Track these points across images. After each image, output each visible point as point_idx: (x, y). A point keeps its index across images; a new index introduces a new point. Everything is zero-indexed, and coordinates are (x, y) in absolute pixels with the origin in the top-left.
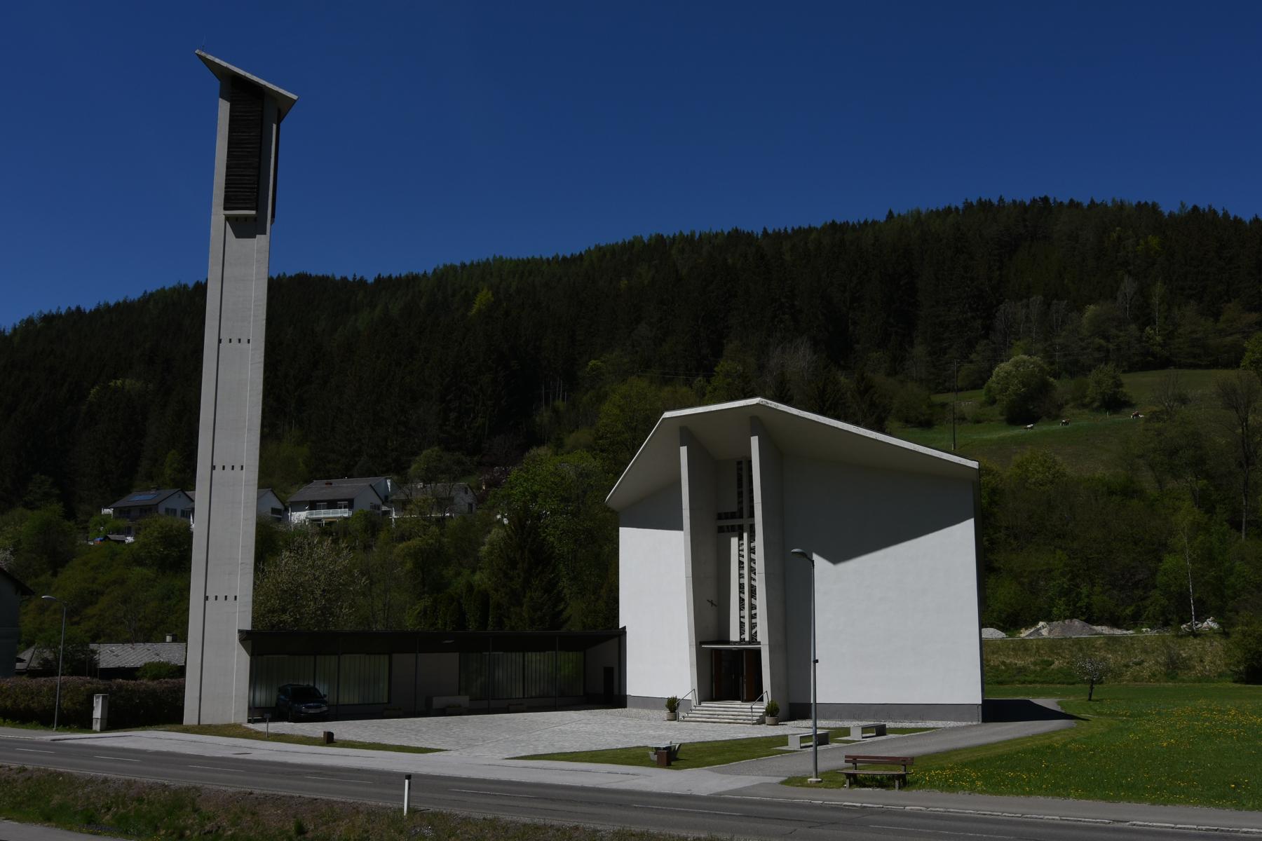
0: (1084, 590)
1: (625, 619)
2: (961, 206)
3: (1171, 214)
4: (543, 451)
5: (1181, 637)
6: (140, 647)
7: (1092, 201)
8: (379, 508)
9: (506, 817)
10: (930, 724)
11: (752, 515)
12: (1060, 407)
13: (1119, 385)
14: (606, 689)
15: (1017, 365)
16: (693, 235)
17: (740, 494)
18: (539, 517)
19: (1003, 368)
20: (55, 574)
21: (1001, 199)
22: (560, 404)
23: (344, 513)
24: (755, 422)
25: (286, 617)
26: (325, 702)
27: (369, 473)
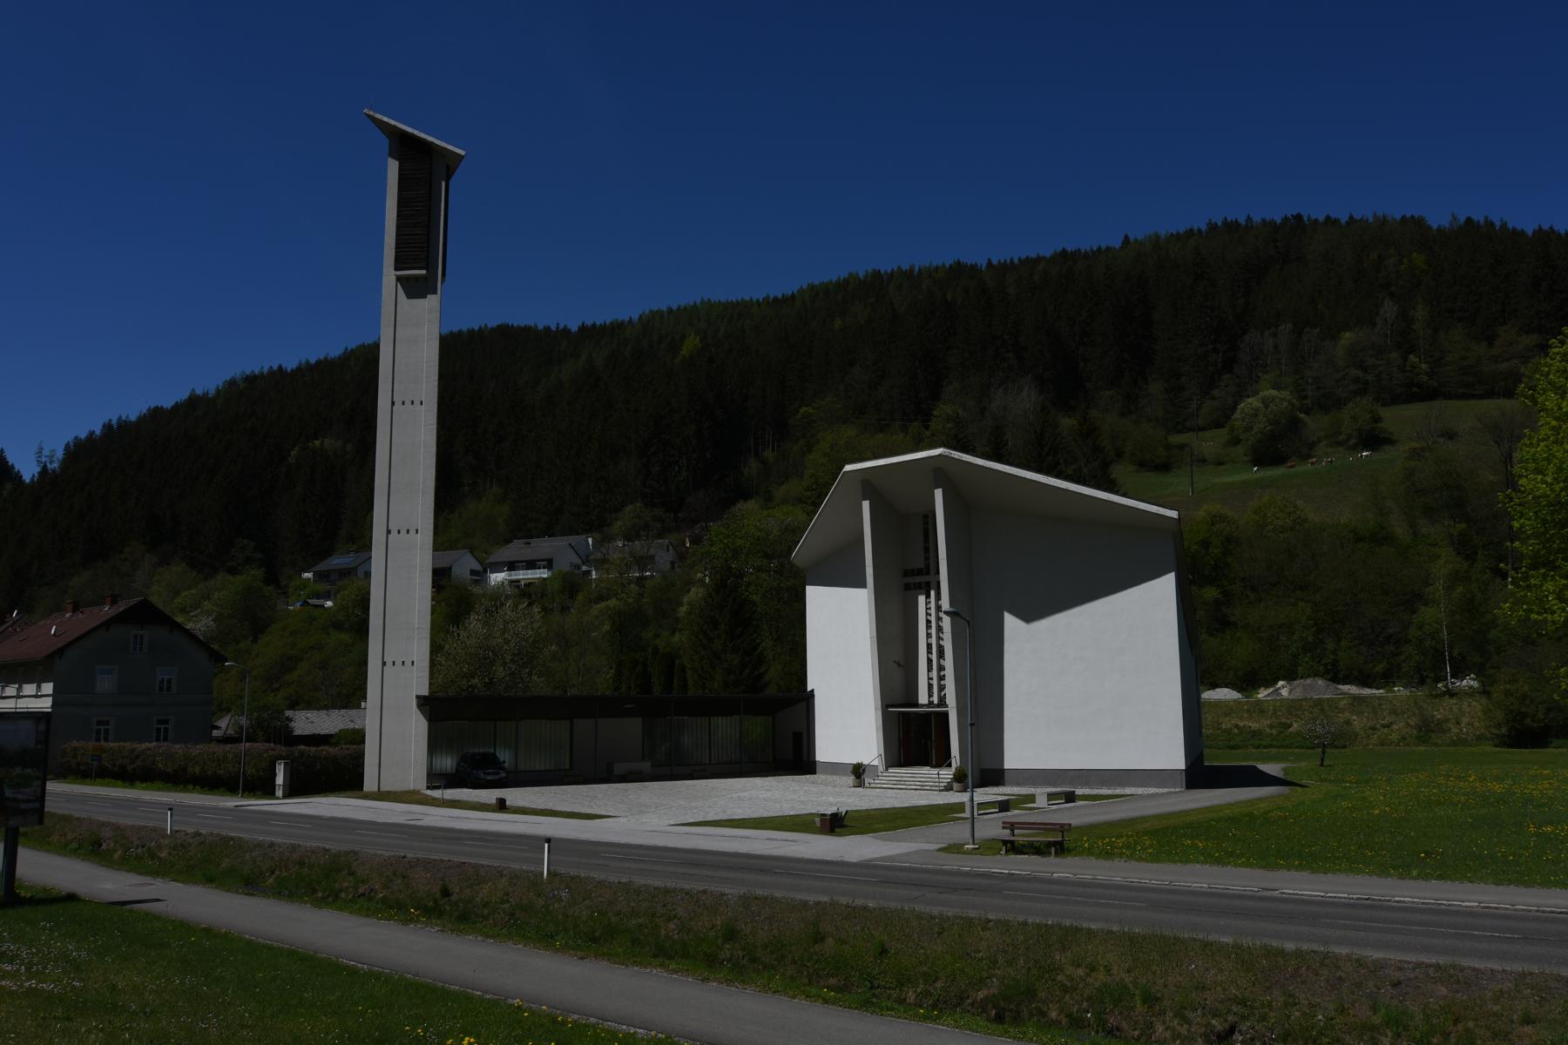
0: (1330, 645)
1: (815, 680)
2: (1204, 228)
3: (1439, 229)
4: (751, 505)
5: (1436, 696)
6: (335, 713)
7: (1351, 217)
8: (579, 567)
9: (640, 881)
10: (1128, 791)
11: (938, 572)
12: (1312, 446)
13: (1377, 420)
14: (793, 753)
15: (1266, 402)
16: (912, 270)
17: (927, 550)
18: (741, 575)
19: (1251, 403)
20: (255, 640)
21: (1249, 219)
22: (769, 455)
23: (544, 574)
24: (939, 473)
25: (476, 681)
26: (503, 769)
27: (573, 531)
